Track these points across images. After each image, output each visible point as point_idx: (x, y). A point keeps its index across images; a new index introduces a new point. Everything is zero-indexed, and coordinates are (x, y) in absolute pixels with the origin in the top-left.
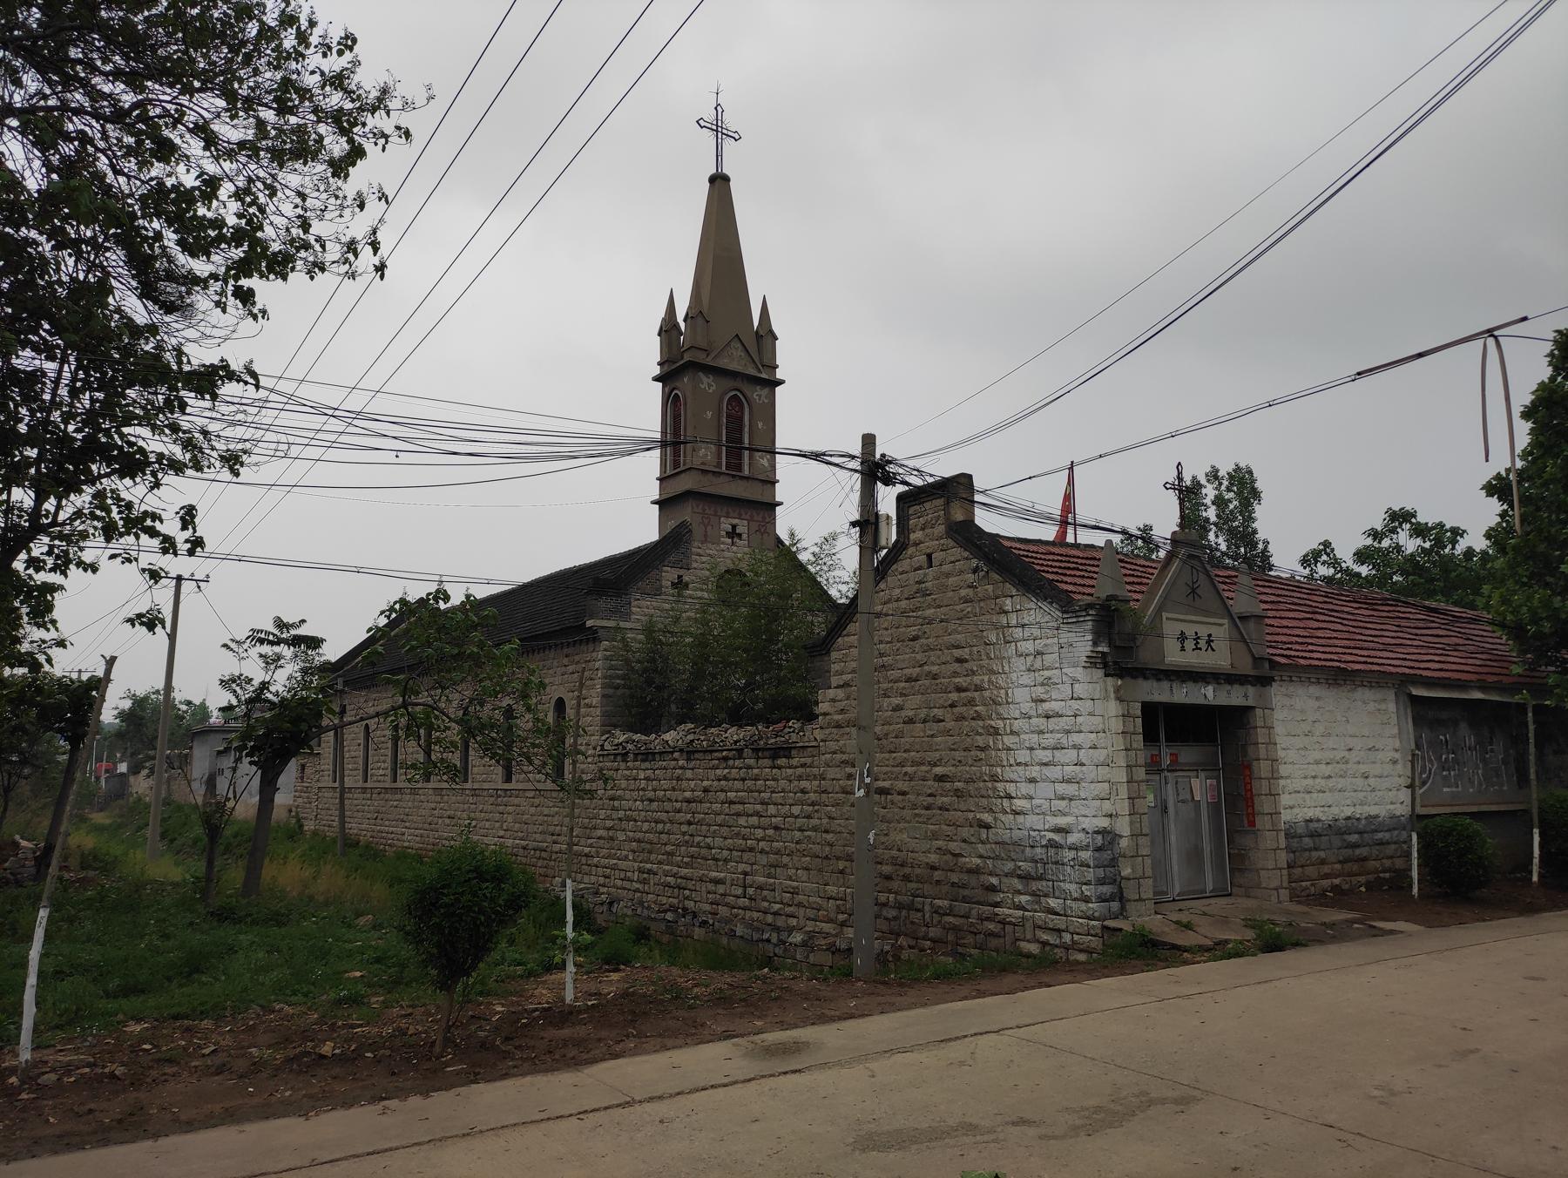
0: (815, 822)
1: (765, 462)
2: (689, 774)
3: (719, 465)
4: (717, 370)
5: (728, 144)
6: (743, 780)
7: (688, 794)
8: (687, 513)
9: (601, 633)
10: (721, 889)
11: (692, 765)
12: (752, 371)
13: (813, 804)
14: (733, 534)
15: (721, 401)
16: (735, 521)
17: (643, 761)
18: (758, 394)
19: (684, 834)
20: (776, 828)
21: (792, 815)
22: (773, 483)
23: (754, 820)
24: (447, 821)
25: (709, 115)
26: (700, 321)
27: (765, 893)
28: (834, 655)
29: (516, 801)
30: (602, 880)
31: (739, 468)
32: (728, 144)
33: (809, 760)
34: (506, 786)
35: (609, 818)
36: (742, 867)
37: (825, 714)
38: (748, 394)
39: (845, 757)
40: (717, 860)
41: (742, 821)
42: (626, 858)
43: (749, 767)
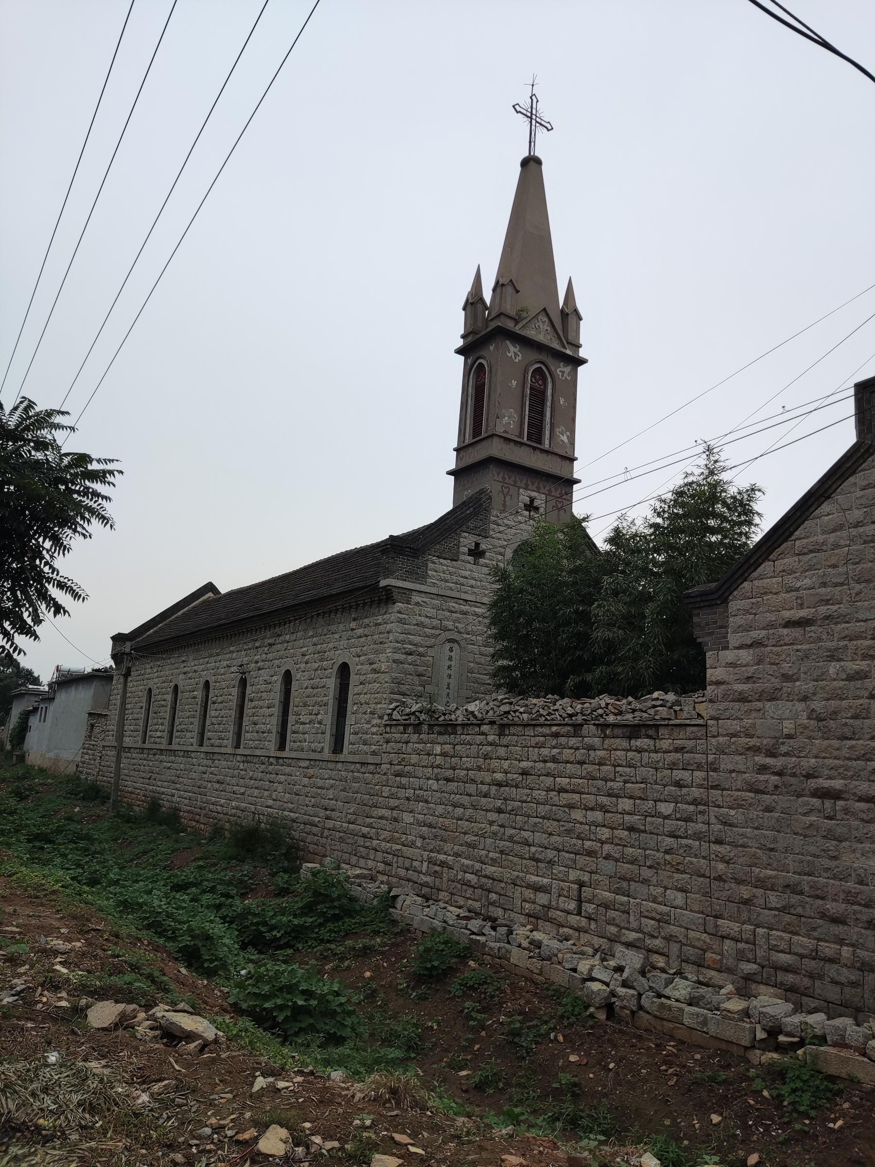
0: (693, 827)
1: (565, 438)
2: (502, 751)
3: (521, 435)
4: (520, 350)
5: (541, 133)
6: (581, 763)
7: (499, 776)
8: (491, 482)
9: (396, 596)
10: (542, 898)
11: (505, 740)
12: (556, 345)
13: (695, 802)
14: (531, 506)
15: (526, 371)
16: (534, 494)
17: (440, 733)
18: (562, 370)
19: (491, 823)
20: (631, 829)
21: (659, 815)
22: (572, 460)
23: (598, 816)
24: (217, 786)
25: (525, 102)
26: (509, 290)
27: (612, 914)
28: (734, 605)
29: (288, 770)
30: (381, 867)
31: (540, 441)
32: (541, 133)
33: (691, 743)
34: (279, 754)
35: (392, 796)
36: (573, 875)
37: (718, 683)
38: (553, 368)
39: (753, 742)
40: (538, 860)
41: (577, 815)
42: (412, 845)
43: (591, 748)
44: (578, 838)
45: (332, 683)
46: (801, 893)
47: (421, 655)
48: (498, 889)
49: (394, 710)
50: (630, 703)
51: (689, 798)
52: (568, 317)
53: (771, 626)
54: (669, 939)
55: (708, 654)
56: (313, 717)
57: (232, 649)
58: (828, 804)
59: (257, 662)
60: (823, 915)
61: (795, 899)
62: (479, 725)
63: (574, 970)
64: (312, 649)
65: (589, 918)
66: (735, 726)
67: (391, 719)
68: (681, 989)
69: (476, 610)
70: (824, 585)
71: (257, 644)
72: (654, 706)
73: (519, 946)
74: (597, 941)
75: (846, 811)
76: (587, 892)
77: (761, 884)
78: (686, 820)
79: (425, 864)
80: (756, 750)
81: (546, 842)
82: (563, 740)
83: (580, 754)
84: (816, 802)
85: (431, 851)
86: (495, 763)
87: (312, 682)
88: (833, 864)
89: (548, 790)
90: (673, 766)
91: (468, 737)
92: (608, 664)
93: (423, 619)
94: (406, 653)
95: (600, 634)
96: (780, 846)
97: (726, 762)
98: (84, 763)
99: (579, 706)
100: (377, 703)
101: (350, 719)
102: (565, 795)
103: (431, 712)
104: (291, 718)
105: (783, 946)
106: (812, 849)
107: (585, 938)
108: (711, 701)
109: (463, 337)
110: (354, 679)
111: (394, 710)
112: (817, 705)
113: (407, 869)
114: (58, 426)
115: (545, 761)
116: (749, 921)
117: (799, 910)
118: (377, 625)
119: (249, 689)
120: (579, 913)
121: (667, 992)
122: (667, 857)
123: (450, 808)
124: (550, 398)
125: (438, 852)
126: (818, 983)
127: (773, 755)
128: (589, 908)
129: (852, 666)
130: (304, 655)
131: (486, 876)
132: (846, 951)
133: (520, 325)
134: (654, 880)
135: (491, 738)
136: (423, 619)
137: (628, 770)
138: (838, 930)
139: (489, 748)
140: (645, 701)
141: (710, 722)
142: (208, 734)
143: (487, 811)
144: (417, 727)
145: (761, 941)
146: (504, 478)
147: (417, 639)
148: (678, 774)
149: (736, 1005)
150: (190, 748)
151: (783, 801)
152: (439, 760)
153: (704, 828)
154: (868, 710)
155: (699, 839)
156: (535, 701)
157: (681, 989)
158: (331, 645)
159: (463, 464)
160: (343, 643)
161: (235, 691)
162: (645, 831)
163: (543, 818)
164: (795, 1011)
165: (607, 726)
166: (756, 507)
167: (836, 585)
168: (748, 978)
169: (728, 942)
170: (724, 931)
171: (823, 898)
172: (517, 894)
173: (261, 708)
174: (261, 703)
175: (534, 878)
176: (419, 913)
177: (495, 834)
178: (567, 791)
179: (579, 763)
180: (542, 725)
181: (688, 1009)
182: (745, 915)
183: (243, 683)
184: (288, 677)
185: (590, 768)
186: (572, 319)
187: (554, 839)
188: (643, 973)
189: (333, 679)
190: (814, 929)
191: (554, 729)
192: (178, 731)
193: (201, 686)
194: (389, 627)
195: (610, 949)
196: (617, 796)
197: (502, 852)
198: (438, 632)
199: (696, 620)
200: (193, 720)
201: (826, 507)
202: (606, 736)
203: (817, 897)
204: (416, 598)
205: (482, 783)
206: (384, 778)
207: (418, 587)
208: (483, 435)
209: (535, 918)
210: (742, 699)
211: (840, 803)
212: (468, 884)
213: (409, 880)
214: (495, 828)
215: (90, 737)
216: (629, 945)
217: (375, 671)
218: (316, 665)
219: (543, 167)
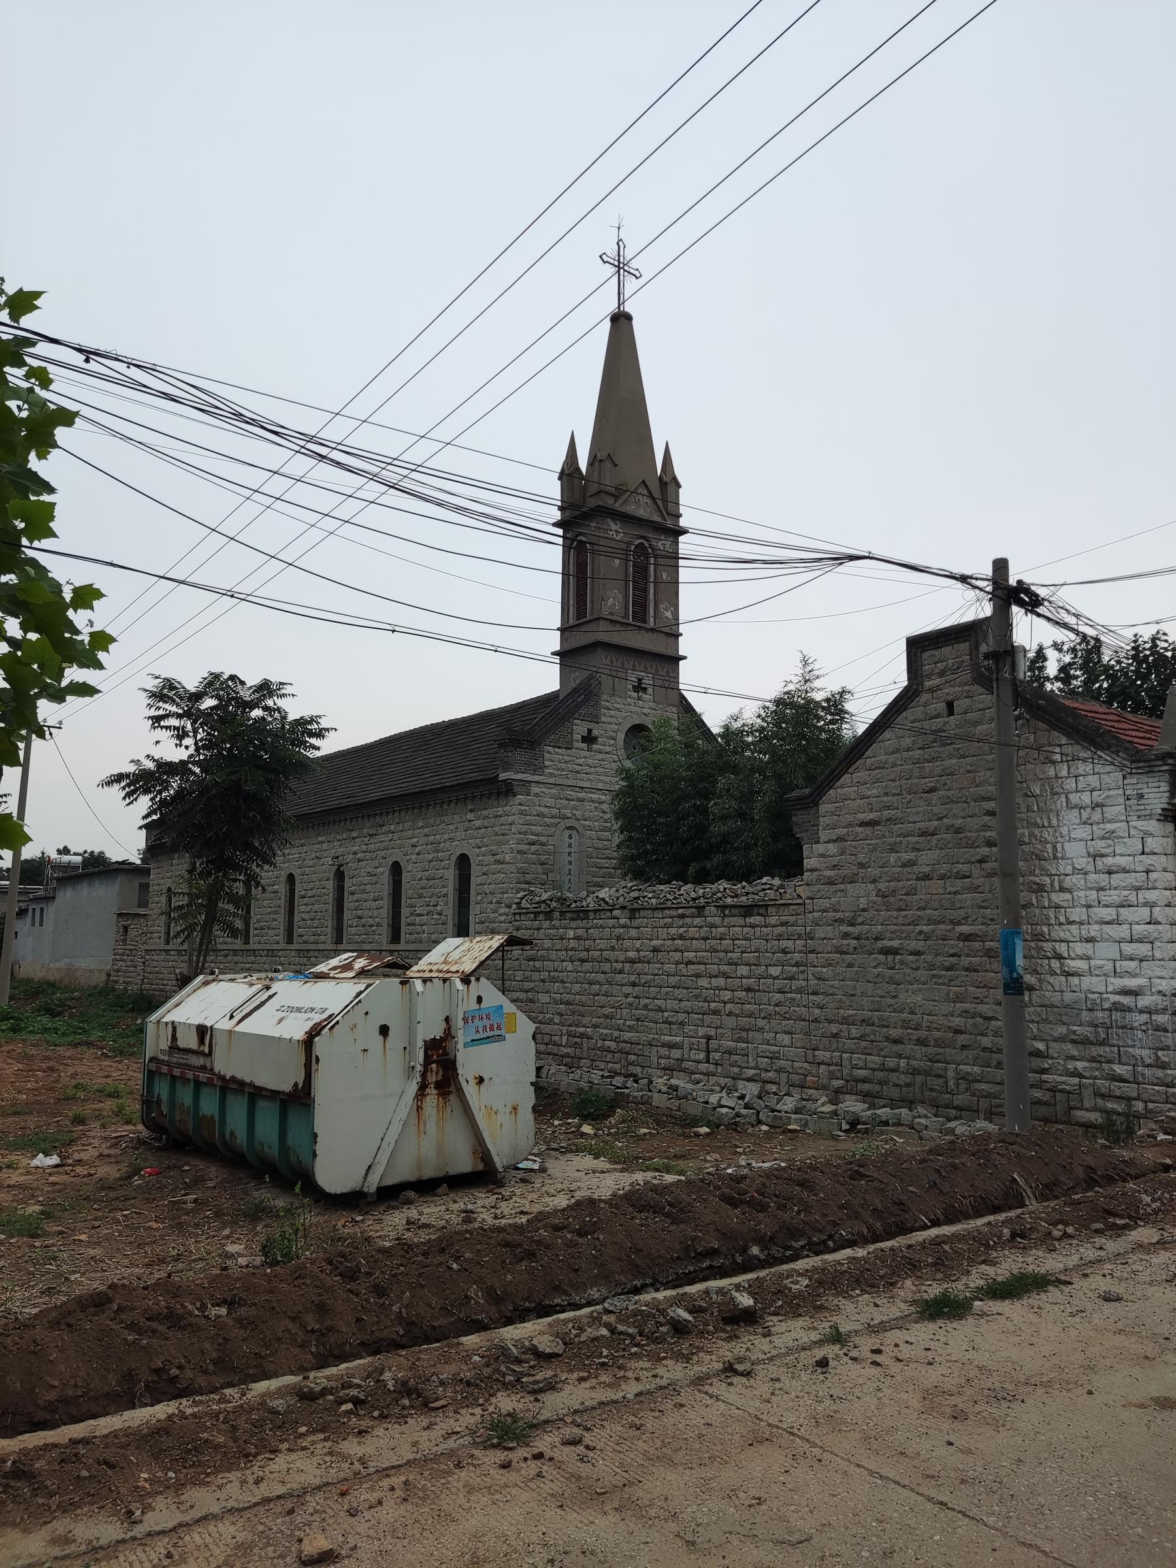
1: (669, 615)
3: (626, 616)
4: (618, 524)
5: (631, 285)
6: (705, 939)
7: (632, 954)
9: (516, 789)
10: (676, 1054)
11: (636, 923)
12: (656, 518)
13: (797, 965)
17: (572, 919)
18: (663, 544)
19: (627, 995)
20: (748, 990)
21: (770, 977)
22: (677, 636)
23: (721, 981)
25: (611, 250)
26: (608, 464)
28: (824, 808)
31: (645, 621)
34: (393, 947)
37: (812, 870)
39: (839, 915)
40: (670, 1023)
41: (703, 982)
42: (550, 1022)
43: (712, 926)
44: (705, 1001)
45: (451, 875)
46: (873, 1025)
47: (543, 844)
48: (636, 1051)
49: (522, 899)
50: (744, 888)
51: (793, 962)
52: (668, 484)
53: (850, 825)
54: (779, 1071)
55: (805, 847)
56: (432, 908)
57: (320, 839)
58: (890, 958)
59: (355, 853)
60: (887, 1039)
61: (869, 1029)
62: (611, 911)
63: (707, 1103)
64: (423, 840)
65: (716, 1064)
66: (826, 903)
67: (519, 908)
68: (789, 1104)
69: (593, 796)
70: (886, 794)
71: (354, 834)
72: (764, 890)
73: (660, 1091)
74: (723, 1081)
75: (902, 962)
76: (713, 1044)
77: (846, 1021)
78: (790, 979)
79: (565, 1038)
80: (841, 921)
81: (677, 1007)
82: (689, 920)
83: (704, 932)
84: (882, 957)
85: (570, 1026)
86: (627, 943)
87: (427, 873)
88: (893, 1001)
89: (677, 963)
90: (779, 938)
91: (601, 922)
92: (724, 853)
93: (542, 809)
94: (530, 844)
95: (717, 828)
96: (858, 992)
97: (820, 932)
98: (118, 971)
99: (701, 891)
100: (502, 893)
101: (474, 910)
102: (692, 967)
103: (562, 900)
104: (405, 911)
105: (861, 1064)
106: (880, 992)
107: (713, 1079)
108: (807, 884)
109: (561, 508)
110: (475, 870)
111: (522, 899)
112: (882, 886)
113: (547, 1044)
114: (284, 695)
115: (673, 939)
116: (837, 1050)
117: (872, 1037)
118: (497, 816)
119: (348, 883)
120: (708, 1062)
121: (779, 1107)
122: (777, 1009)
123: (586, 986)
124: (652, 574)
125: (577, 1026)
126: (885, 1087)
127: (853, 925)
128: (716, 1056)
129: (905, 856)
130: (414, 846)
131: (624, 1042)
132: (903, 1063)
133: (620, 501)
134: (767, 1028)
135: (622, 921)
136: (542, 809)
137: (744, 942)
138: (897, 1048)
139: (622, 930)
140: (756, 885)
141: (807, 901)
142: (297, 931)
143: (622, 985)
144: (549, 915)
145: (846, 1063)
146: (612, 662)
147: (538, 829)
148: (784, 944)
149: (828, 1108)
150: (276, 947)
151: (859, 958)
152: (573, 944)
153: (804, 983)
154: (915, 889)
155: (801, 993)
156: (661, 887)
157: (789, 1104)
158: (446, 836)
159: (568, 647)
160: (460, 834)
161: (330, 885)
162: (759, 991)
163: (674, 987)
164: (869, 1109)
165: (726, 907)
166: (848, 706)
167: (895, 795)
168: (838, 1091)
169: (822, 1067)
170: (819, 1059)
171: (887, 1027)
172: (654, 1053)
173: (366, 901)
174: (365, 896)
175: (668, 1038)
176: (565, 1078)
177: (631, 1005)
178: (694, 963)
179: (703, 939)
180: (669, 909)
181: (793, 1116)
182: (834, 1046)
183: (340, 876)
184: (396, 869)
185: (713, 942)
186: (671, 488)
187: (683, 1004)
188: (760, 1097)
189: (452, 870)
190: (882, 1050)
191: (680, 911)
192: (256, 929)
193: (283, 878)
194: (510, 819)
195: (734, 1085)
196: (736, 964)
197: (638, 1020)
198: (557, 820)
199: (794, 819)
200: (275, 916)
201: (887, 734)
202: (725, 916)
203: (884, 1026)
204: (535, 789)
205: (616, 961)
206: (517, 963)
207: (536, 778)
208: (588, 617)
209: (669, 1070)
210: (831, 882)
211: (898, 957)
212: (608, 1050)
213: (549, 1054)
214: (630, 1000)
215: (124, 941)
216: (749, 1080)
217: (499, 862)
218: (431, 856)
219: (634, 322)
